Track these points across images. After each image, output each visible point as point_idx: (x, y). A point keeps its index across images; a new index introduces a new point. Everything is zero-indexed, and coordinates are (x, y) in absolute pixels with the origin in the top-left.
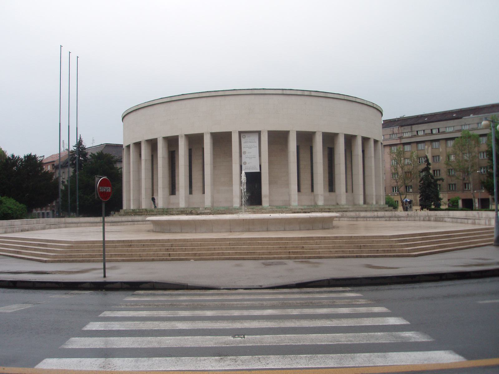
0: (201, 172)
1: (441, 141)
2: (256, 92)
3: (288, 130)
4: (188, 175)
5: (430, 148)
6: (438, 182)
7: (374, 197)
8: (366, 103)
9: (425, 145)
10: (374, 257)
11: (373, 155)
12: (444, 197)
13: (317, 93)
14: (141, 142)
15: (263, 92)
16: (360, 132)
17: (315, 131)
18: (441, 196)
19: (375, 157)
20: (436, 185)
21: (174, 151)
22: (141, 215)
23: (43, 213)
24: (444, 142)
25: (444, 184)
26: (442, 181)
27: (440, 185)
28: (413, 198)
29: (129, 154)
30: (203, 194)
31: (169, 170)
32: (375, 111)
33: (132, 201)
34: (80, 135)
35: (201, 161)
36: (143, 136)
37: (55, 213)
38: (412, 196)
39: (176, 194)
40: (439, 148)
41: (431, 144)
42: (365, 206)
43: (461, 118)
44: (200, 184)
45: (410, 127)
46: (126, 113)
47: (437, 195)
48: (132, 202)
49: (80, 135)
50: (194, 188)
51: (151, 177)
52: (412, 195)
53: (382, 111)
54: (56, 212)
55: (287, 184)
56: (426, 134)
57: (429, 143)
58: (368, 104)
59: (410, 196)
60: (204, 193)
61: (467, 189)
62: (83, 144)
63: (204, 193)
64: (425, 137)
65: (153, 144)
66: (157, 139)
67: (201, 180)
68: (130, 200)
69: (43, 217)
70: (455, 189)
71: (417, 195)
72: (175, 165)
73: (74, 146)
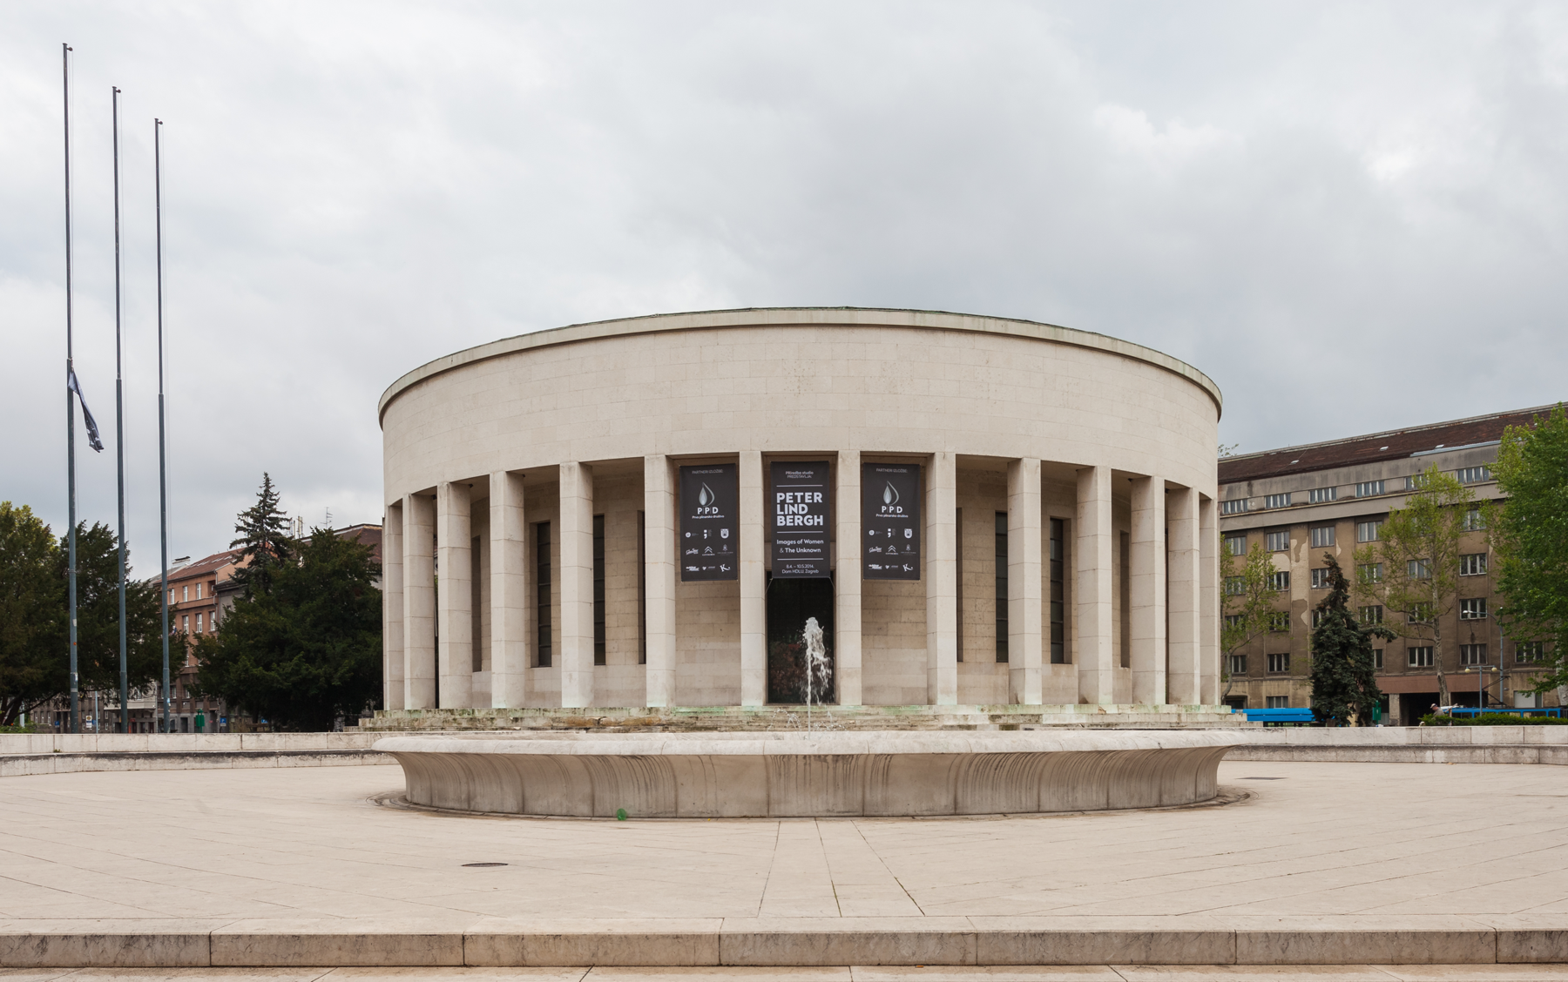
0: (634, 593)
1: (1340, 526)
2: (821, 317)
3: (930, 451)
4: (591, 599)
5: (1305, 546)
6: (1376, 643)
7: (1197, 681)
8: (1181, 372)
9: (1290, 539)
10: (73, 439)
11: (1196, 545)
12: (1392, 684)
13: (1025, 325)
14: (435, 488)
15: (845, 317)
16: (1160, 472)
17: (1019, 457)
18: (59, 695)
19: (1201, 551)
20: (1366, 652)
21: (547, 523)
22: (1221, 618)
23: (185, 720)
24: (1350, 526)
25: (1393, 652)
26: (1386, 639)
27: (1379, 652)
28: (1247, 690)
29: (400, 534)
30: (640, 663)
31: (531, 584)
32: (1206, 398)
33: (407, 683)
34: (266, 475)
35: (633, 555)
36: (442, 471)
37: (218, 719)
38: (1244, 686)
39: (553, 665)
40: (1334, 546)
41: (1309, 534)
42: (1173, 708)
43: (1407, 456)
44: (632, 632)
45: (1244, 485)
46: (388, 397)
47: (1366, 679)
48: (409, 688)
49: (266, 475)
50: (610, 646)
51: (468, 605)
52: (1247, 683)
53: (1220, 402)
54: (222, 717)
55: (923, 637)
56: (1292, 505)
57: (1302, 532)
58: (1187, 375)
59: (1239, 684)
60: (645, 662)
61: (1416, 665)
62: (278, 507)
63: (643, 660)
64: (1291, 512)
65: (474, 493)
66: (487, 477)
67: (635, 619)
68: (402, 681)
69: (185, 730)
70: (1430, 662)
71: (1262, 681)
72: (550, 569)
73: (247, 514)
